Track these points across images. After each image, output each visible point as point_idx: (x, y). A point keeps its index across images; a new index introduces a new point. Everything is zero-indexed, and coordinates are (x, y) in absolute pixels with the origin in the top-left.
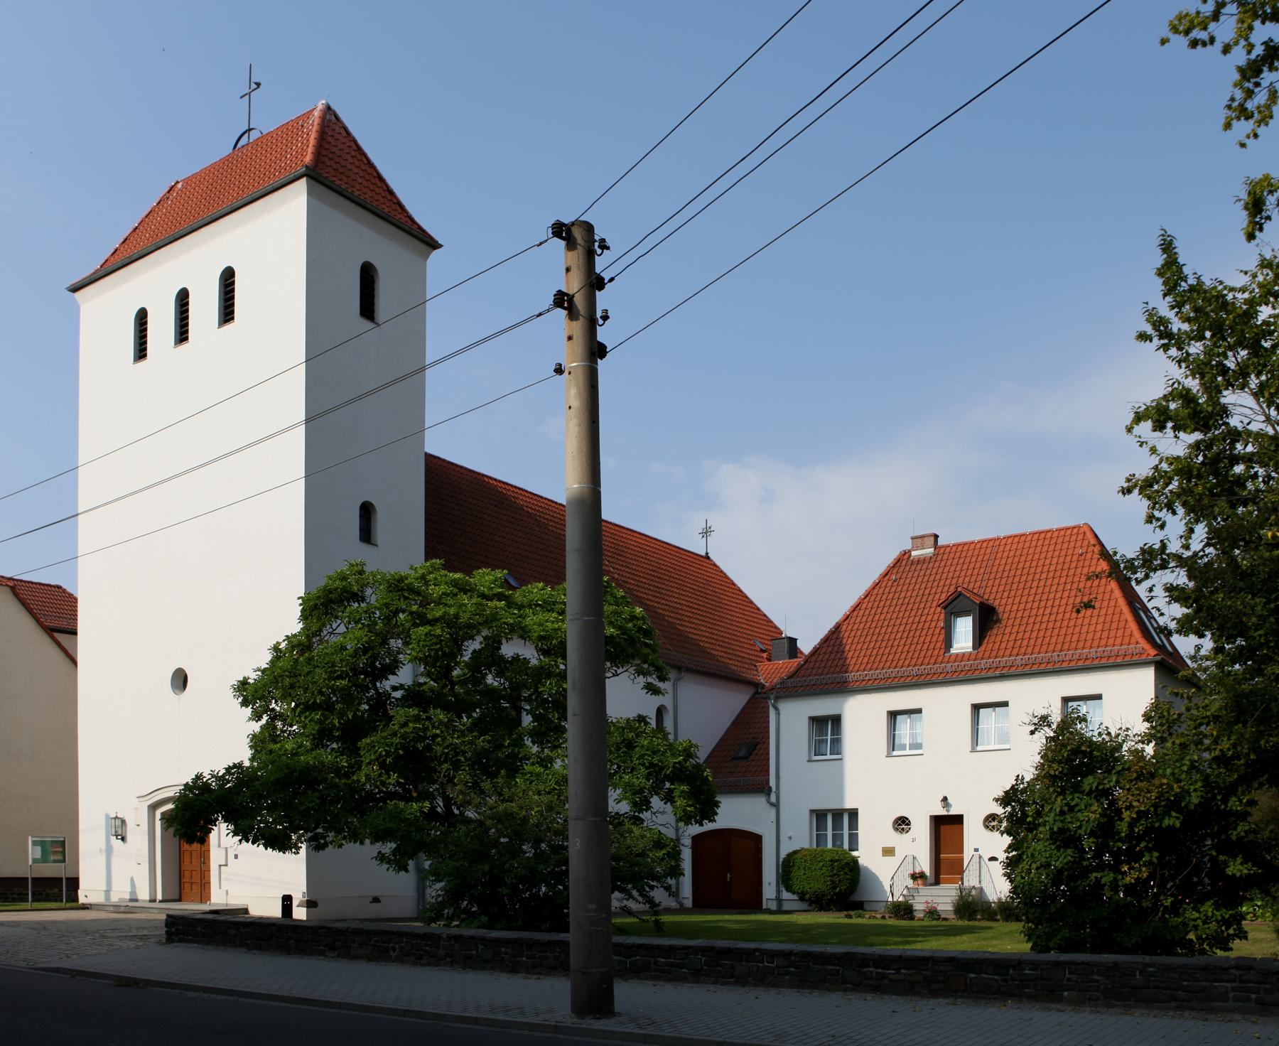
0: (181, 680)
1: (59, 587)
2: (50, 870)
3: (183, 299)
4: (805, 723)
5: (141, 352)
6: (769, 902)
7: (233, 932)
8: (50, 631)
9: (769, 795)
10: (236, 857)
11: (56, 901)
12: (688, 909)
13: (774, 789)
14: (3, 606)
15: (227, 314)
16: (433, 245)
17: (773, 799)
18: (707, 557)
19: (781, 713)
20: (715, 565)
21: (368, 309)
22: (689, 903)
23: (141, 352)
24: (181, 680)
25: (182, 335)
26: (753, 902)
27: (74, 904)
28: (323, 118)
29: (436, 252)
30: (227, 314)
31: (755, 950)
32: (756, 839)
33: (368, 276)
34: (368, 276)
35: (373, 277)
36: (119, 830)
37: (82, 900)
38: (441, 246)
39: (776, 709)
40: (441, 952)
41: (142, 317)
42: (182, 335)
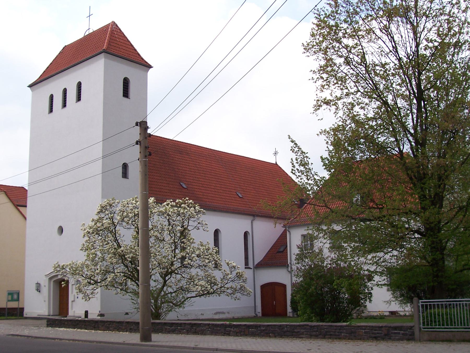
0: (61, 230)
1: (23, 188)
2: (13, 305)
3: (65, 91)
4: (300, 236)
5: (51, 110)
6: (290, 313)
7: (66, 323)
8: (17, 206)
9: (288, 267)
10: (78, 298)
11: (16, 316)
12: (260, 317)
13: (289, 265)
14: (1, 198)
15: (79, 98)
16: (149, 67)
17: (289, 269)
18: (276, 164)
19: (291, 233)
20: (279, 167)
21: (126, 94)
22: (260, 315)
23: (51, 110)
24: (61, 230)
25: (64, 105)
26: (284, 314)
27: (22, 317)
28: (112, 31)
29: (151, 69)
30: (79, 98)
31: (201, 323)
32: (284, 286)
33: (126, 82)
34: (126, 82)
35: (128, 82)
36: (38, 288)
37: (25, 316)
38: (153, 67)
39: (289, 232)
40: (124, 327)
41: (52, 97)
42: (64, 105)
